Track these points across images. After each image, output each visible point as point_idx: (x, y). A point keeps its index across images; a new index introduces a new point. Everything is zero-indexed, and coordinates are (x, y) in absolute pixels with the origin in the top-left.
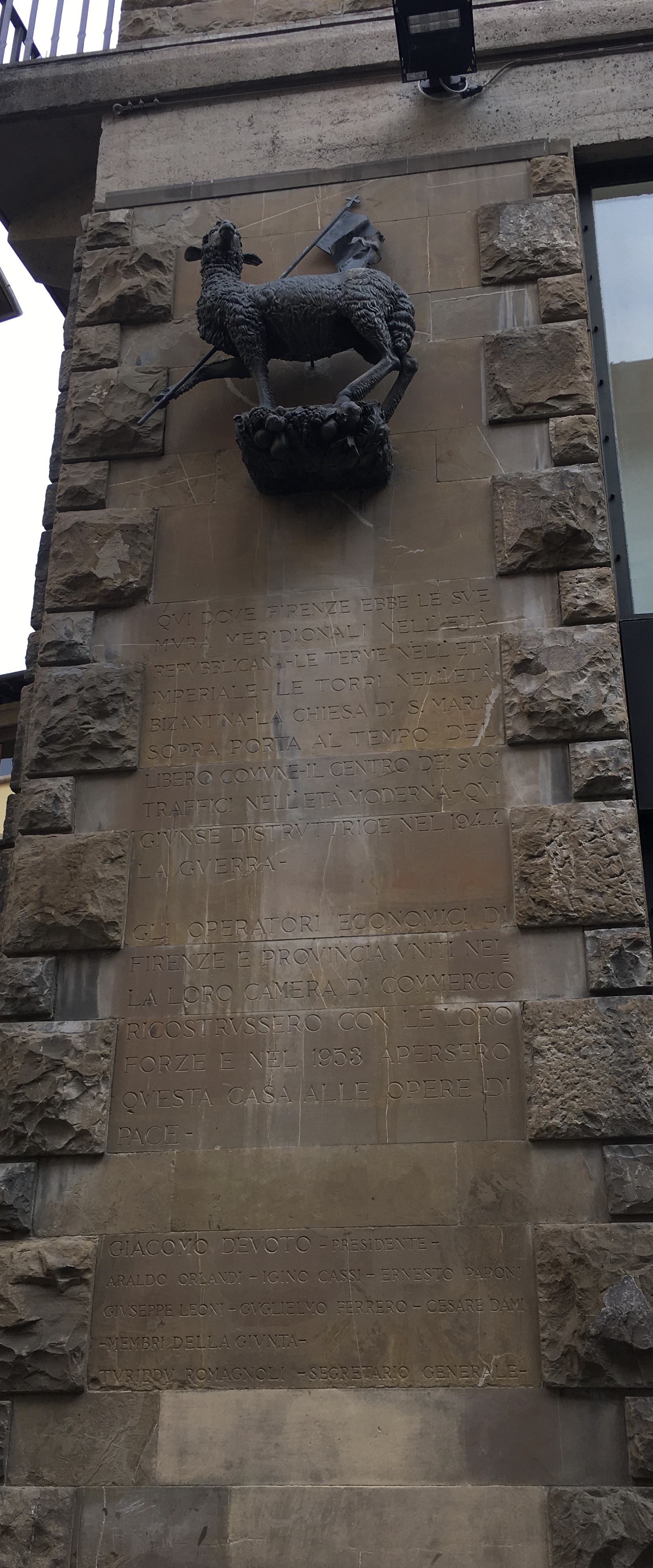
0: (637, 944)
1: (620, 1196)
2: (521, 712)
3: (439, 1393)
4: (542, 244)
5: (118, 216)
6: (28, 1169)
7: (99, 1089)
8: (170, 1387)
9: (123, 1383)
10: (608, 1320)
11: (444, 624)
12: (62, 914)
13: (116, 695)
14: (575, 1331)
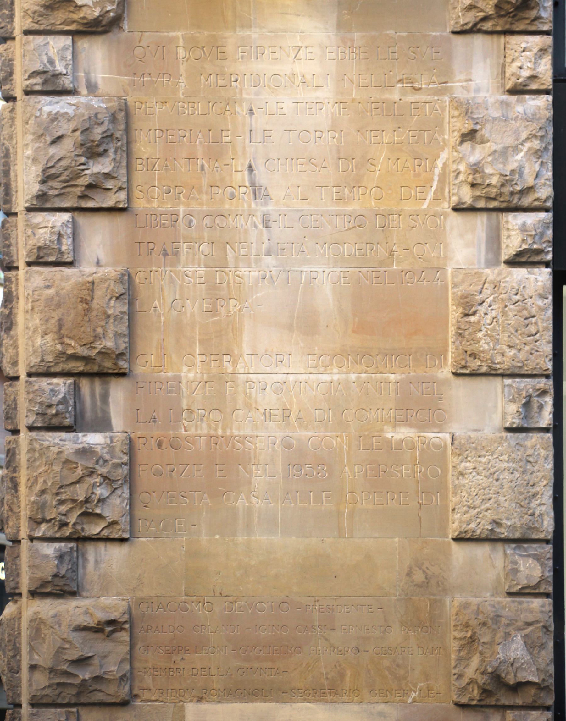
0: (543, 393)
1: (514, 581)
2: (466, 181)
3: (381, 707)
6: (71, 548)
7: (123, 489)
9: (157, 698)
10: (500, 663)
11: (400, 81)
12: (81, 346)
13: (107, 137)
14: (477, 670)
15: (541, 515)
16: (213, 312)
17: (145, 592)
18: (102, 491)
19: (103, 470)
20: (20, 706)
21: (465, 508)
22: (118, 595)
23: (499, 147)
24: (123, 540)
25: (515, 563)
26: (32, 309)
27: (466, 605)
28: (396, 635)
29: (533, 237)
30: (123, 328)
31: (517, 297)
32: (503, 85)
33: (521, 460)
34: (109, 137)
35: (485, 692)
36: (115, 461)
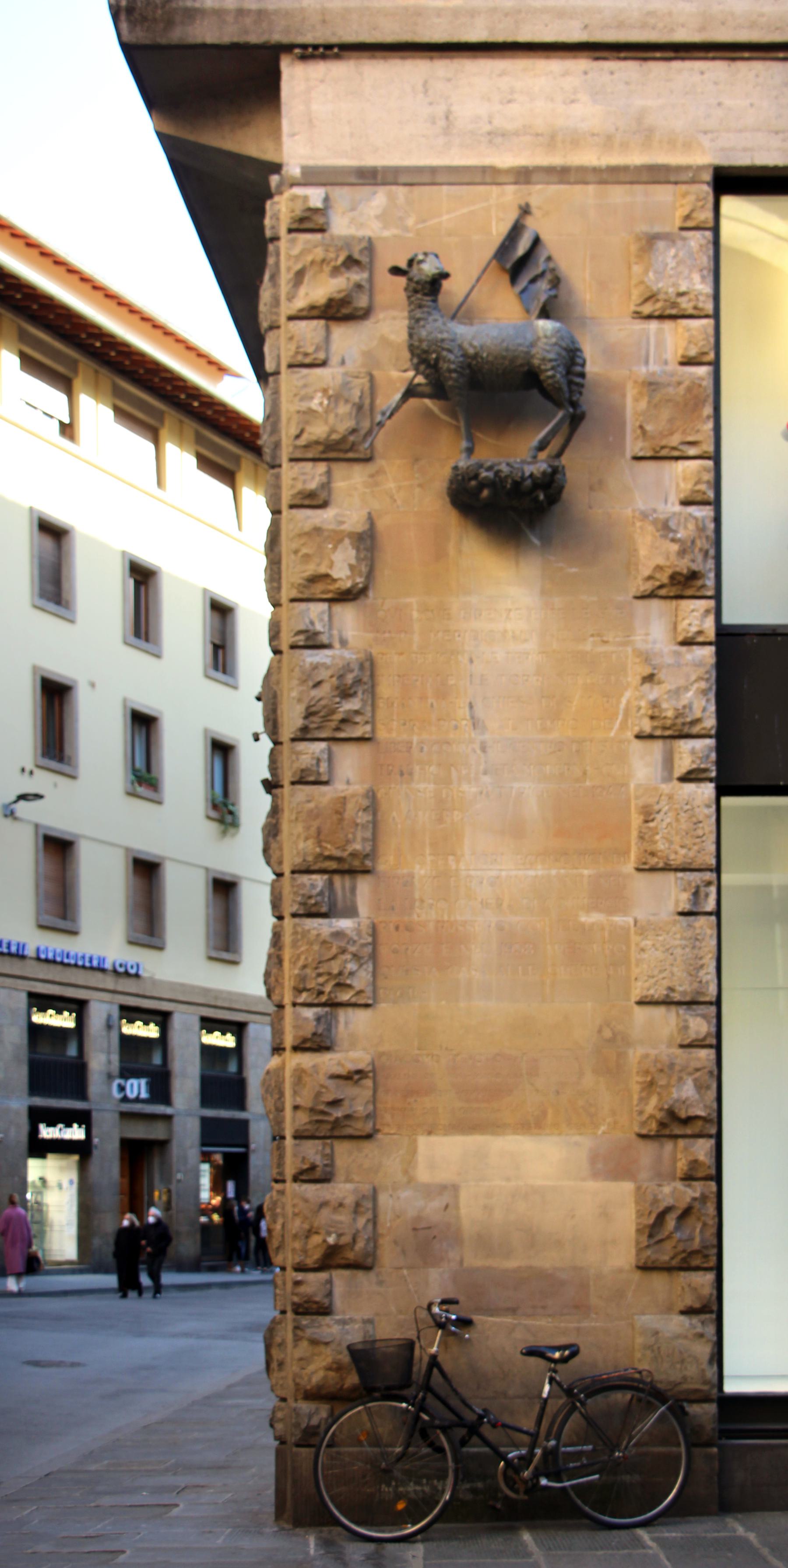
0: (709, 884)
3: (577, 1138)
4: (683, 288)
5: (315, 196)
6: (327, 1012)
8: (422, 1134)
11: (592, 635)
15: (707, 982)
16: (440, 820)
17: (385, 1048)
18: (351, 966)
19: (353, 949)
20: (283, 1138)
21: (646, 978)
22: (364, 1049)
23: (673, 687)
24: (367, 1006)
25: (686, 1021)
26: (297, 819)
27: (647, 1056)
28: (589, 1080)
29: (701, 758)
30: (368, 834)
31: (688, 807)
32: (675, 638)
33: (691, 938)
34: (358, 681)
35: (662, 1125)
36: (363, 941)
